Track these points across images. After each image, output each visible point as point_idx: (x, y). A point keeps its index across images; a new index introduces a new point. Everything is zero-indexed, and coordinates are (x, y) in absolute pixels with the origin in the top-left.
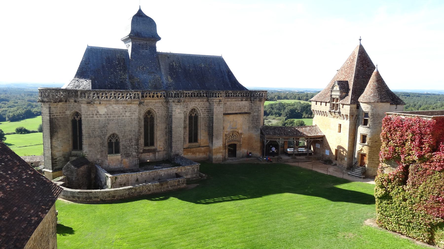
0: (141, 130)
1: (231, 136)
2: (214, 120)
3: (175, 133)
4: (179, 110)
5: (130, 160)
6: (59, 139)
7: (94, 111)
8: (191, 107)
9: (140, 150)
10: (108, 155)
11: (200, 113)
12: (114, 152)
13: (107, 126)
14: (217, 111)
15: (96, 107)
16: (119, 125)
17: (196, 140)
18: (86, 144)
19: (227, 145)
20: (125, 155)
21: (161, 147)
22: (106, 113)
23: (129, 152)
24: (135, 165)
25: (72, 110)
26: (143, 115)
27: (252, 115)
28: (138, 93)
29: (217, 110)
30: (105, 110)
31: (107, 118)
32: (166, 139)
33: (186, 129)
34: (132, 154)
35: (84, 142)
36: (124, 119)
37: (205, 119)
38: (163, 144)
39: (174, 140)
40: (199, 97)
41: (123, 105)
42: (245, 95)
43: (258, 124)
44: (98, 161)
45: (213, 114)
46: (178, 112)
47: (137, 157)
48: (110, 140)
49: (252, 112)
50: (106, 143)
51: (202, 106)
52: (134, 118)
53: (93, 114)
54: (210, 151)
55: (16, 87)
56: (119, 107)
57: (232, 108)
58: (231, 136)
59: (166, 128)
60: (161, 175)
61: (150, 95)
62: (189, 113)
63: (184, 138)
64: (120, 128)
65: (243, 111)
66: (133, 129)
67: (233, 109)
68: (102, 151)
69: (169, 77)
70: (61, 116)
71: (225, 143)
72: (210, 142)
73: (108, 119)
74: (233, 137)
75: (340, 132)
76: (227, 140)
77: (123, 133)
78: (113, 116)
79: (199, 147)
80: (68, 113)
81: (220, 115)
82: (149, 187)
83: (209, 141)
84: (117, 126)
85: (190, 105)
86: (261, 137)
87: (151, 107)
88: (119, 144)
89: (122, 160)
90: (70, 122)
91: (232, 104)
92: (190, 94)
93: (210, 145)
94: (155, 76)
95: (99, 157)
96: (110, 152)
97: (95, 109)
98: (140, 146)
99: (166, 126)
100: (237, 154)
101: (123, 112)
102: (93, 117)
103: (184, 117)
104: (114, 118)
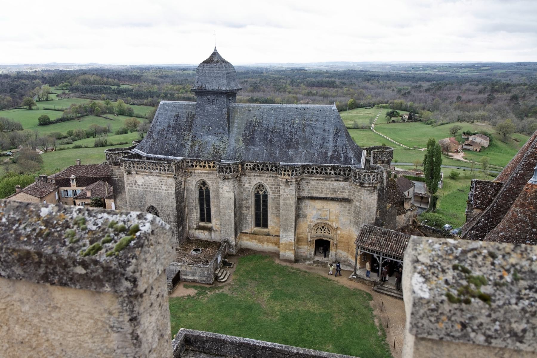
4: (227, 188)
8: (256, 183)
13: (145, 197)
26: (195, 187)
29: (285, 192)
30: (143, 180)
36: (161, 192)
40: (265, 170)
41: (159, 178)
42: (342, 173)
46: (225, 191)
52: (171, 193)
53: (132, 184)
55: (109, 67)
64: (157, 201)
65: (341, 196)
67: (322, 191)
69: (241, 138)
79: (268, 235)
92: (252, 166)
94: (222, 137)
102: (132, 186)
104: (152, 190)
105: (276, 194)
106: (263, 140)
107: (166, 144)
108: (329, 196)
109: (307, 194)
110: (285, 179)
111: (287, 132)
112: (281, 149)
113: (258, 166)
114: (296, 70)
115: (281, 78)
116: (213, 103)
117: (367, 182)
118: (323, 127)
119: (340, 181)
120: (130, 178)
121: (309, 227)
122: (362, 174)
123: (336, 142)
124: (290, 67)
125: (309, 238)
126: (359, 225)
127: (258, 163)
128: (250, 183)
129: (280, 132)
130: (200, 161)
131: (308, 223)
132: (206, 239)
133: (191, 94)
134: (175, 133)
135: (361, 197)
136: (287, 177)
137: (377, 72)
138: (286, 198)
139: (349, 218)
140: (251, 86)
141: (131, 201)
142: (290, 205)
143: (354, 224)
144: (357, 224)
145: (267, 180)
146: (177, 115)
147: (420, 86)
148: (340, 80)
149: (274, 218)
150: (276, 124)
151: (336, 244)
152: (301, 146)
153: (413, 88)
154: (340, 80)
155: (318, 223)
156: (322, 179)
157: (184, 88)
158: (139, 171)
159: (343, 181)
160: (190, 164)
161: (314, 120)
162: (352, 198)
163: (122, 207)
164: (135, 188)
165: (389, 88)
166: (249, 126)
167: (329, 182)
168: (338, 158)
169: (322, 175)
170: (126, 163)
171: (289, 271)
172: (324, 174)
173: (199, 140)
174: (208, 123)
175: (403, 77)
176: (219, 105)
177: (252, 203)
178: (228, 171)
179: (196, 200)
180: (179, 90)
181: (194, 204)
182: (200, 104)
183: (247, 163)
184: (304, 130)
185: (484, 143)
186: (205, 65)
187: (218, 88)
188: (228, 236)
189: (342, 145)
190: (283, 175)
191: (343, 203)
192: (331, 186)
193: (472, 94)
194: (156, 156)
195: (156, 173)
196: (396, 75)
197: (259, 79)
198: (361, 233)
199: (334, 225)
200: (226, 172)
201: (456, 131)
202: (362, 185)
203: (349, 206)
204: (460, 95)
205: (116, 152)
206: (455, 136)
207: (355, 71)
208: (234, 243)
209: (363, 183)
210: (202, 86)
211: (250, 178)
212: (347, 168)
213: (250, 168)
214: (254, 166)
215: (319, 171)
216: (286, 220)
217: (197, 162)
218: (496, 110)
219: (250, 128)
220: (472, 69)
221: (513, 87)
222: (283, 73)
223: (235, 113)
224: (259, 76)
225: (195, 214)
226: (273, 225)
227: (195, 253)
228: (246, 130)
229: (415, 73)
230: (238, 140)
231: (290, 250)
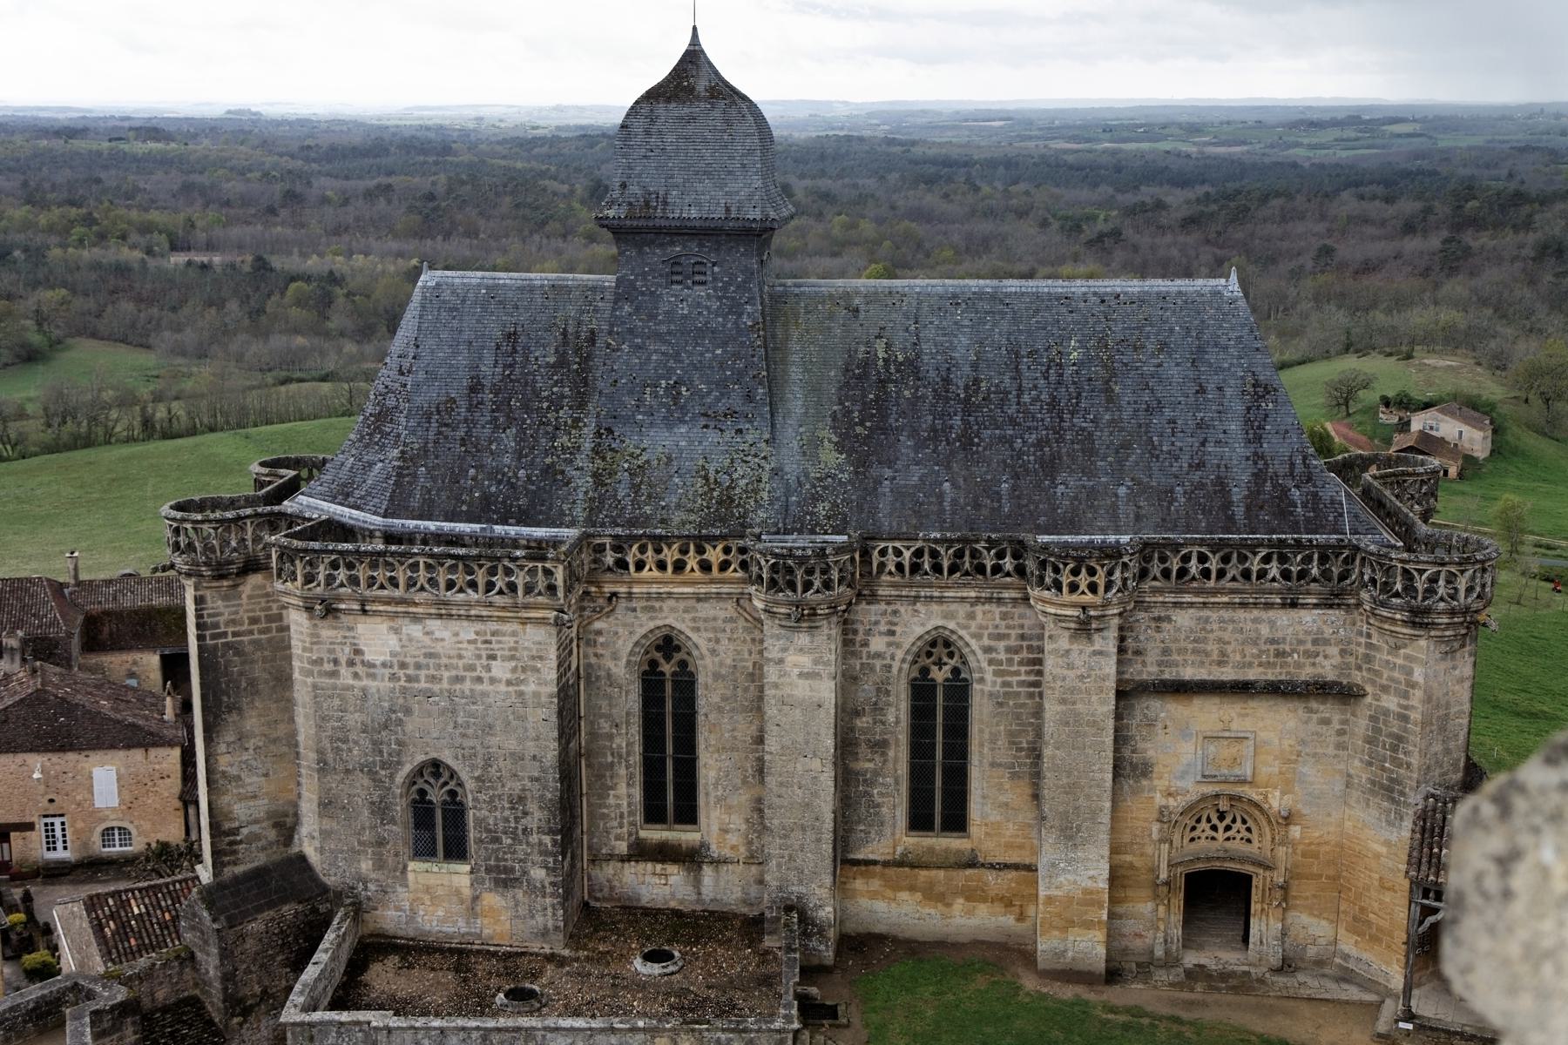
1: (1209, 820)
3: (781, 784)
4: (805, 661)
5: (516, 905)
6: (251, 744)
7: (341, 643)
8: (919, 631)
9: (613, 843)
10: (412, 865)
13: (400, 722)
15: (350, 629)
16: (460, 720)
18: (310, 800)
20: (494, 875)
21: (733, 839)
22: (395, 660)
23: (509, 863)
24: (543, 935)
26: (629, 662)
27: (1371, 705)
29: (1070, 666)
30: (393, 642)
31: (402, 683)
34: (525, 873)
36: (484, 694)
37: (1011, 703)
38: (744, 827)
39: (776, 822)
40: (967, 573)
41: (479, 626)
42: (1315, 571)
43: (1402, 771)
44: (365, 883)
46: (796, 671)
47: (552, 895)
49: (1373, 683)
50: (396, 805)
51: (997, 627)
52: (536, 695)
53: (336, 662)
55: (998, 107)
56: (457, 634)
57: (1212, 647)
58: (1209, 820)
61: (661, 556)
64: (464, 735)
65: (1306, 674)
66: (531, 748)
67: (1223, 654)
68: (381, 843)
69: (827, 434)
70: (256, 636)
73: (405, 688)
77: (480, 762)
78: (427, 676)
79: (972, 864)
81: (1094, 698)
84: (450, 729)
85: (913, 616)
87: (673, 617)
89: (476, 899)
91: (1215, 626)
92: (907, 554)
94: (739, 431)
95: (366, 866)
96: (424, 851)
97: (345, 637)
98: (615, 824)
101: (479, 657)
104: (436, 688)
105: (1015, 679)
106: (929, 438)
107: (472, 472)
108: (1252, 675)
109: (1154, 669)
110: (1074, 605)
111: (1036, 400)
112: (1016, 476)
113: (934, 554)
114: (604, 135)
115: (543, 174)
116: (697, 278)
117: (1442, 605)
118: (1191, 374)
119: (1304, 606)
120: (327, 632)
121: (1162, 815)
122: (1421, 572)
123: (1258, 439)
124: (572, 122)
125: (1164, 866)
126: (1402, 794)
127: (936, 541)
128: (892, 633)
129: (1003, 403)
130: (659, 542)
131: (1159, 800)
132: (673, 904)
133: (125, 250)
134: (511, 420)
135: (1410, 672)
136: (1089, 598)
137: (960, 146)
138: (1073, 690)
139: (1342, 766)
140: (411, 209)
141: (326, 744)
143: (1372, 792)
144: (1389, 790)
145: (971, 616)
146: (512, 337)
147: (1160, 205)
148: (808, 182)
149: (1000, 787)
150: (983, 365)
151: (1285, 888)
152: (1104, 459)
153: (1131, 211)
154: (808, 182)
155: (1204, 798)
156: (1225, 599)
157: (89, 221)
158: (375, 600)
159: (1316, 606)
160: (609, 558)
161: (1150, 347)
162: (1358, 680)
163: (239, 778)
164: (351, 682)
165: (1022, 214)
166: (859, 377)
167: (1256, 613)
168: (1282, 506)
169: (1226, 583)
170: (310, 563)
171: (1105, 1023)
172: (1234, 579)
173: (630, 444)
174: (670, 371)
175: (1071, 167)
176: (725, 289)
177: (897, 722)
178: (817, 584)
179: (628, 723)
180: (66, 231)
181: (620, 742)
182: (632, 283)
183: (883, 545)
184: (1108, 390)
185: (1471, 440)
186: (661, 109)
187: (728, 210)
188: (801, 882)
189: (1284, 451)
190: (1065, 589)
192: (1265, 631)
193: (1373, 238)
194: (432, 525)
195: (468, 605)
196: (1042, 156)
197: (442, 178)
198: (1423, 830)
199: (1276, 802)
200: (807, 586)
201: (1350, 392)
202: (1419, 619)
203: (1343, 712)
204: (1328, 242)
205: (229, 515)
206: (1349, 415)
207: (861, 139)
208: (829, 909)
209: (1427, 611)
210: (647, 204)
211: (895, 612)
212: (1339, 547)
213: (900, 567)
214: (919, 553)
215: (1214, 564)
216: (1071, 789)
217: (643, 549)
218: (1484, 302)
219: (863, 389)
220: (1350, 133)
221: (1537, 205)
222: (545, 149)
223: (786, 324)
224: (436, 163)
225: (622, 789)
226: (995, 817)
227: (655, 969)
228: (847, 398)
229: (1121, 151)
230: (816, 443)
231: (1088, 925)
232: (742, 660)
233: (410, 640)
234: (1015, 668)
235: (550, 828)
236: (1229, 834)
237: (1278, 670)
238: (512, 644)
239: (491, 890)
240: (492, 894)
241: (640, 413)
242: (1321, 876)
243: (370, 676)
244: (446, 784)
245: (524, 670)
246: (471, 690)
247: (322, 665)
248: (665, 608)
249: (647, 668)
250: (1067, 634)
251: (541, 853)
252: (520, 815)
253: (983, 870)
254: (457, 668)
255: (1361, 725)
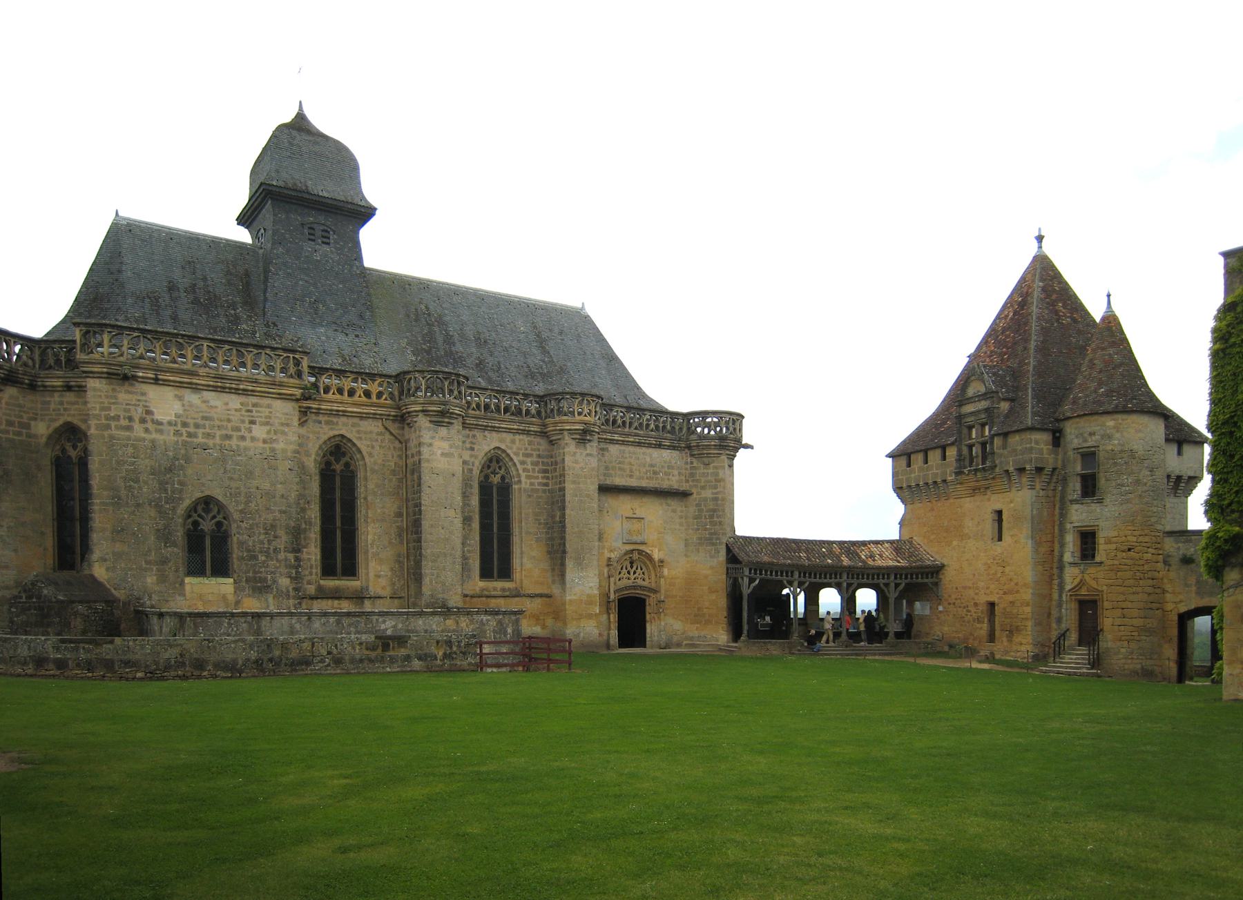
0: (309, 513)
2: (568, 498)
4: (445, 445)
7: (135, 405)
8: (487, 449)
10: (187, 580)
11: (519, 475)
12: (208, 572)
13: (182, 468)
14: (577, 466)
15: (143, 394)
16: (228, 467)
17: (505, 572)
19: (612, 597)
21: (383, 582)
22: (179, 420)
23: (263, 575)
25: (56, 420)
26: (315, 459)
28: (296, 356)
30: (177, 407)
31: (184, 438)
32: (399, 556)
33: (470, 525)
34: (274, 581)
35: (97, 521)
36: (246, 449)
37: (535, 495)
38: (390, 573)
39: (429, 551)
41: (243, 399)
42: (668, 427)
45: (563, 475)
47: (294, 598)
48: (196, 524)
49: (696, 486)
50: (177, 531)
51: (526, 449)
52: (284, 451)
53: (130, 419)
54: (558, 613)
56: (227, 404)
57: (627, 467)
59: (399, 515)
60: (383, 630)
62: (481, 471)
63: (465, 558)
64: (231, 479)
68: (164, 561)
70: (11, 436)
71: (607, 591)
72: (556, 578)
73: (186, 442)
74: (635, 573)
75: (1000, 539)
76: (612, 580)
77: (242, 499)
78: (203, 433)
80: (42, 429)
82: (336, 646)
83: (553, 576)
86: (727, 573)
87: (344, 428)
88: (229, 543)
90: (47, 463)
91: (628, 455)
93: (556, 590)
96: (196, 569)
97: (139, 400)
98: (307, 573)
99: (399, 508)
100: (648, 636)
102: (129, 428)
103: (464, 480)
104: (211, 443)
105: (536, 481)
128: (472, 449)
142: (588, 496)
143: (700, 544)
145: (513, 442)
164: (143, 435)
191: (669, 501)
199: (656, 555)
231: (590, 616)
232: (388, 461)
233: (191, 405)
234: (536, 474)
235: (293, 548)
236: (635, 575)
237: (654, 482)
238: (267, 414)
239: (249, 596)
240: (251, 599)
241: (294, 316)
242: (676, 596)
243: (157, 431)
244: (214, 517)
245: (275, 432)
246: (238, 446)
247: (118, 420)
248: (340, 423)
249: (324, 467)
250: (574, 442)
251: (286, 567)
252: (272, 538)
253: (524, 599)
254: (226, 428)
255: (692, 510)
